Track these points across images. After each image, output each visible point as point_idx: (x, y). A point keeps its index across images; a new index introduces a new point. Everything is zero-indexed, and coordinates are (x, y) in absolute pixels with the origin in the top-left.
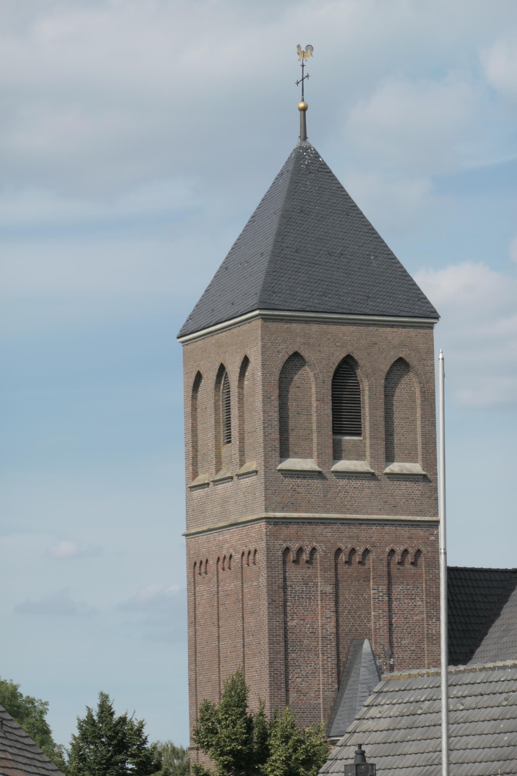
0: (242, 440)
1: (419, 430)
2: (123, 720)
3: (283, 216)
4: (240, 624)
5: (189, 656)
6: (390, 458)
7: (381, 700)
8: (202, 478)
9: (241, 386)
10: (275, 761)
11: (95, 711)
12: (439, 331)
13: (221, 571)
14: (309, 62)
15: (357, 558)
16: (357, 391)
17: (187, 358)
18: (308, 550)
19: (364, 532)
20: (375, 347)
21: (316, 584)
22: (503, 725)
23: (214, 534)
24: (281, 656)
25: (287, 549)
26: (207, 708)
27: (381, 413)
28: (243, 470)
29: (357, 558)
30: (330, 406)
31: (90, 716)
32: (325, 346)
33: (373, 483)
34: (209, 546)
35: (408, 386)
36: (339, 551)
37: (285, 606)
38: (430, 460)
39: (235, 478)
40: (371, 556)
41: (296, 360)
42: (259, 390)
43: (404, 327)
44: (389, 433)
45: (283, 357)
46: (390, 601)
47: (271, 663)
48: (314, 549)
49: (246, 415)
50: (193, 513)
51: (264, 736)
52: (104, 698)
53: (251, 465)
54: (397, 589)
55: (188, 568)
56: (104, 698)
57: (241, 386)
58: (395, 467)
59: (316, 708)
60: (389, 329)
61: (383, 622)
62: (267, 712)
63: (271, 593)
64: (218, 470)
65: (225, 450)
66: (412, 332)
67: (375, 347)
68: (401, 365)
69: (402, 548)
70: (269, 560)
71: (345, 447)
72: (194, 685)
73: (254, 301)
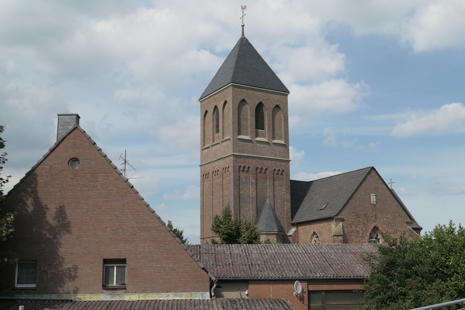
0: (223, 130)
1: (283, 129)
3: (238, 56)
4: (221, 193)
5: (201, 207)
6: (274, 138)
10: (244, 237)
12: (289, 96)
13: (214, 176)
14: (245, 11)
15: (263, 171)
18: (247, 167)
21: (250, 179)
23: (212, 164)
24: (238, 204)
25: (240, 166)
26: (217, 217)
27: (271, 122)
28: (224, 140)
29: (263, 171)
32: (254, 98)
34: (209, 168)
35: (279, 115)
36: (257, 168)
37: (239, 186)
38: (287, 140)
39: (221, 143)
40: (268, 171)
42: (231, 111)
43: (278, 94)
44: (274, 130)
45: (239, 100)
47: (234, 206)
48: (249, 167)
50: (203, 158)
51: (238, 229)
54: (276, 183)
55: (201, 177)
57: (223, 111)
60: (274, 95)
63: (234, 181)
64: (213, 142)
65: (216, 135)
66: (281, 97)
69: (278, 169)
73: (230, 81)
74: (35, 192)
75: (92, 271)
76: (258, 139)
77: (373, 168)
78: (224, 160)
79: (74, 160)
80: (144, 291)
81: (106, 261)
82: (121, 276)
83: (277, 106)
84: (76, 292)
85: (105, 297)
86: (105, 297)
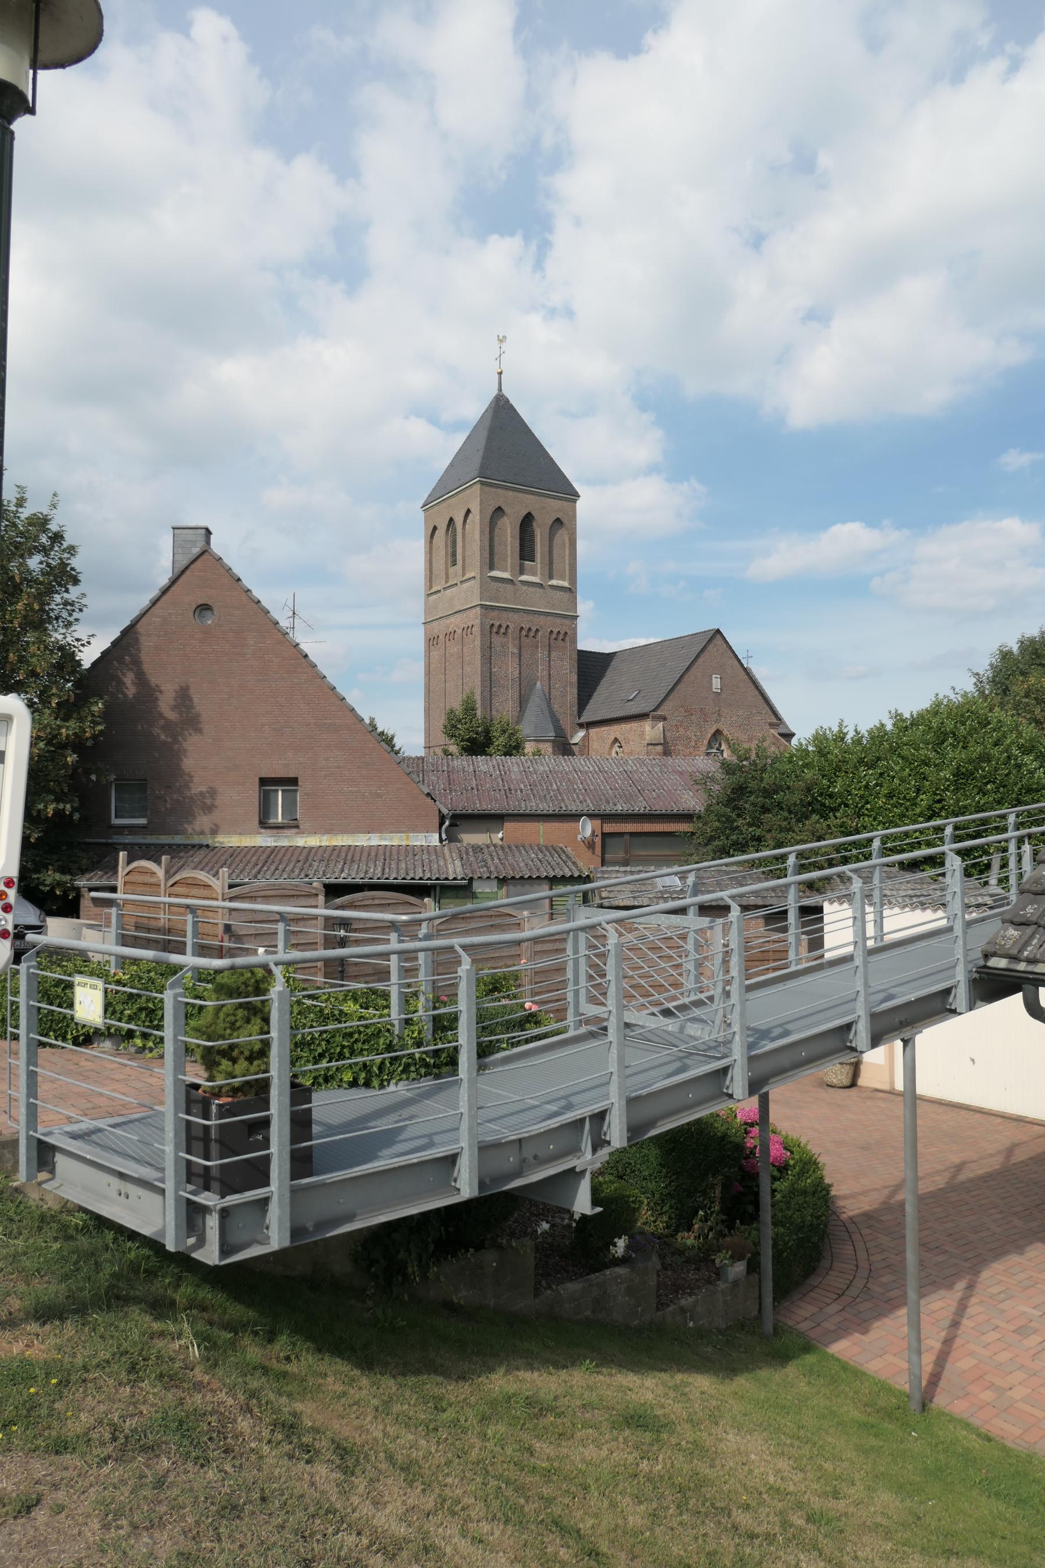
6: (551, 577)
9: (464, 528)
12: (580, 504)
14: (504, 346)
15: (532, 634)
18: (504, 626)
20: (544, 510)
23: (444, 620)
26: (452, 711)
27: (547, 549)
29: (532, 634)
30: (518, 541)
32: (517, 505)
34: (438, 628)
35: (562, 535)
38: (573, 579)
40: (540, 633)
44: (551, 563)
45: (491, 509)
49: (467, 545)
50: (428, 610)
51: (487, 731)
54: (553, 654)
57: (464, 528)
61: (545, 673)
63: (482, 650)
65: (452, 570)
66: (565, 504)
70: (482, 631)
71: (526, 567)
74: (137, 663)
75: (240, 797)
76: (524, 578)
77: (718, 631)
78: (464, 615)
79: (204, 608)
80: (330, 831)
81: (263, 781)
82: (290, 806)
83: (558, 521)
84: (214, 832)
85: (264, 840)
86: (264, 840)
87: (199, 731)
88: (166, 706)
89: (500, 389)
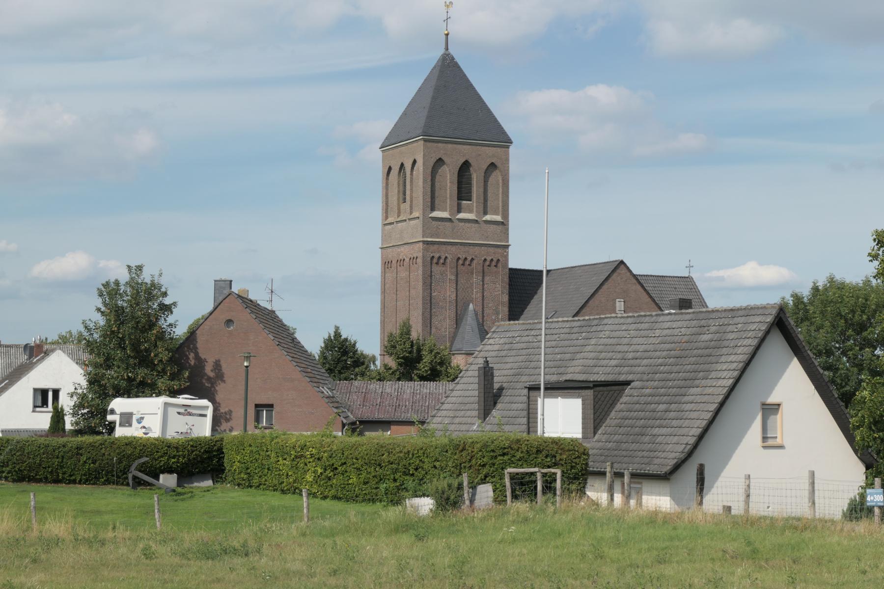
0: (411, 201)
2: (346, 340)
6: (485, 213)
7: (495, 335)
8: (390, 220)
9: (412, 174)
11: (332, 334)
12: (512, 149)
14: (451, 10)
15: (467, 263)
16: (470, 178)
17: (384, 159)
18: (443, 257)
19: (472, 250)
20: (480, 156)
22: (557, 350)
23: (396, 248)
24: (428, 310)
27: (482, 190)
28: (412, 216)
29: (467, 263)
31: (330, 337)
33: (477, 225)
34: (392, 254)
35: (496, 177)
36: (459, 258)
38: (506, 215)
40: (475, 262)
41: (440, 162)
42: (421, 176)
44: (485, 200)
45: (434, 160)
46: (483, 285)
48: (446, 257)
50: (385, 237)
51: (419, 350)
52: (337, 328)
53: (416, 214)
54: (487, 279)
56: (337, 328)
57: (412, 174)
58: (488, 217)
59: (445, 336)
61: (480, 295)
62: (421, 338)
65: (402, 206)
66: (499, 150)
67: (480, 156)
68: (493, 166)
72: (383, 323)
73: (420, 131)
76: (462, 216)
77: (622, 262)
78: (411, 247)
79: (229, 322)
80: (542, 283)
81: (257, 406)
82: (269, 418)
87: (224, 381)
88: (209, 370)
89: (447, 49)
